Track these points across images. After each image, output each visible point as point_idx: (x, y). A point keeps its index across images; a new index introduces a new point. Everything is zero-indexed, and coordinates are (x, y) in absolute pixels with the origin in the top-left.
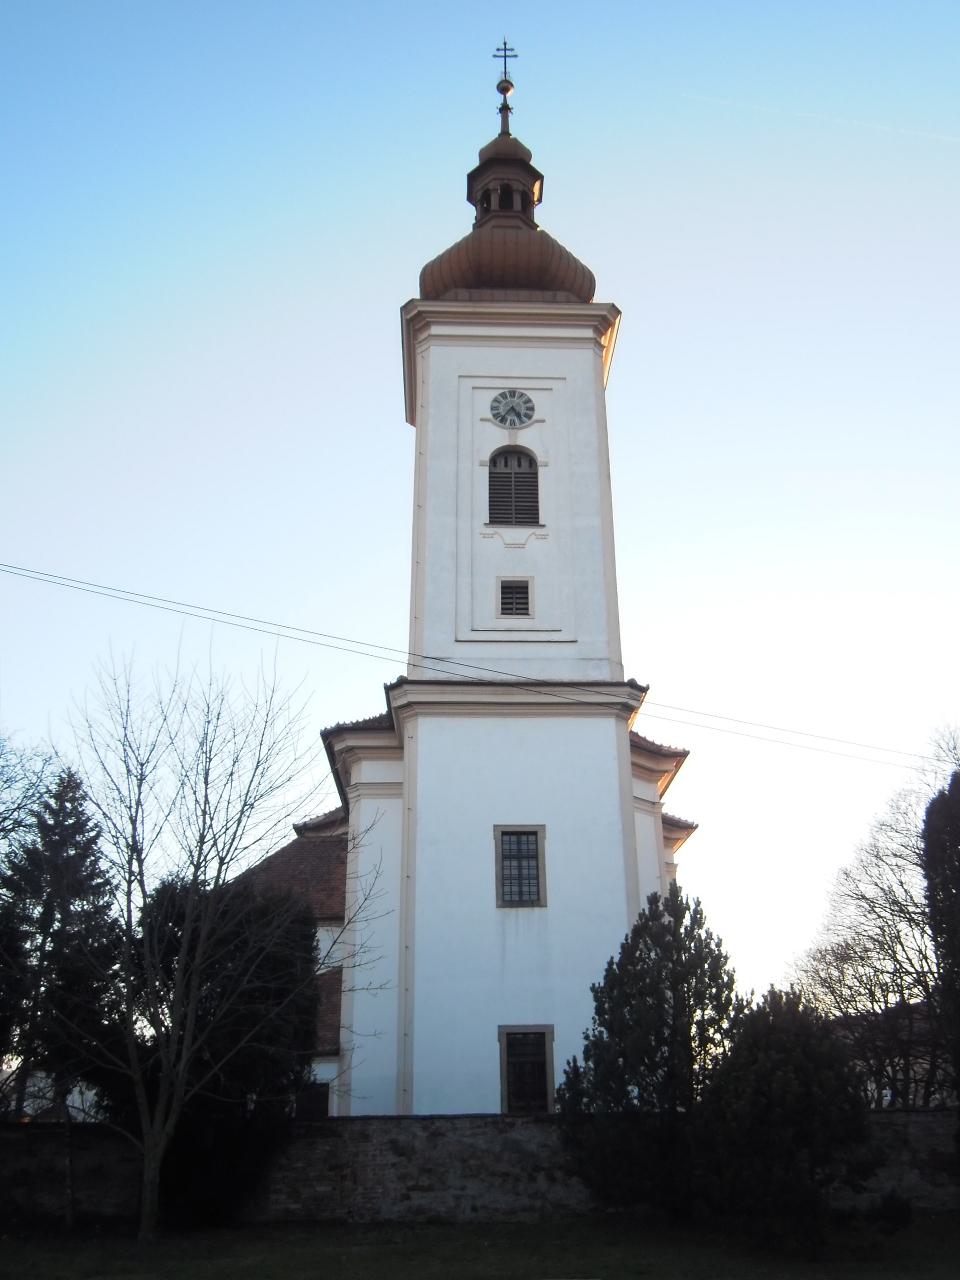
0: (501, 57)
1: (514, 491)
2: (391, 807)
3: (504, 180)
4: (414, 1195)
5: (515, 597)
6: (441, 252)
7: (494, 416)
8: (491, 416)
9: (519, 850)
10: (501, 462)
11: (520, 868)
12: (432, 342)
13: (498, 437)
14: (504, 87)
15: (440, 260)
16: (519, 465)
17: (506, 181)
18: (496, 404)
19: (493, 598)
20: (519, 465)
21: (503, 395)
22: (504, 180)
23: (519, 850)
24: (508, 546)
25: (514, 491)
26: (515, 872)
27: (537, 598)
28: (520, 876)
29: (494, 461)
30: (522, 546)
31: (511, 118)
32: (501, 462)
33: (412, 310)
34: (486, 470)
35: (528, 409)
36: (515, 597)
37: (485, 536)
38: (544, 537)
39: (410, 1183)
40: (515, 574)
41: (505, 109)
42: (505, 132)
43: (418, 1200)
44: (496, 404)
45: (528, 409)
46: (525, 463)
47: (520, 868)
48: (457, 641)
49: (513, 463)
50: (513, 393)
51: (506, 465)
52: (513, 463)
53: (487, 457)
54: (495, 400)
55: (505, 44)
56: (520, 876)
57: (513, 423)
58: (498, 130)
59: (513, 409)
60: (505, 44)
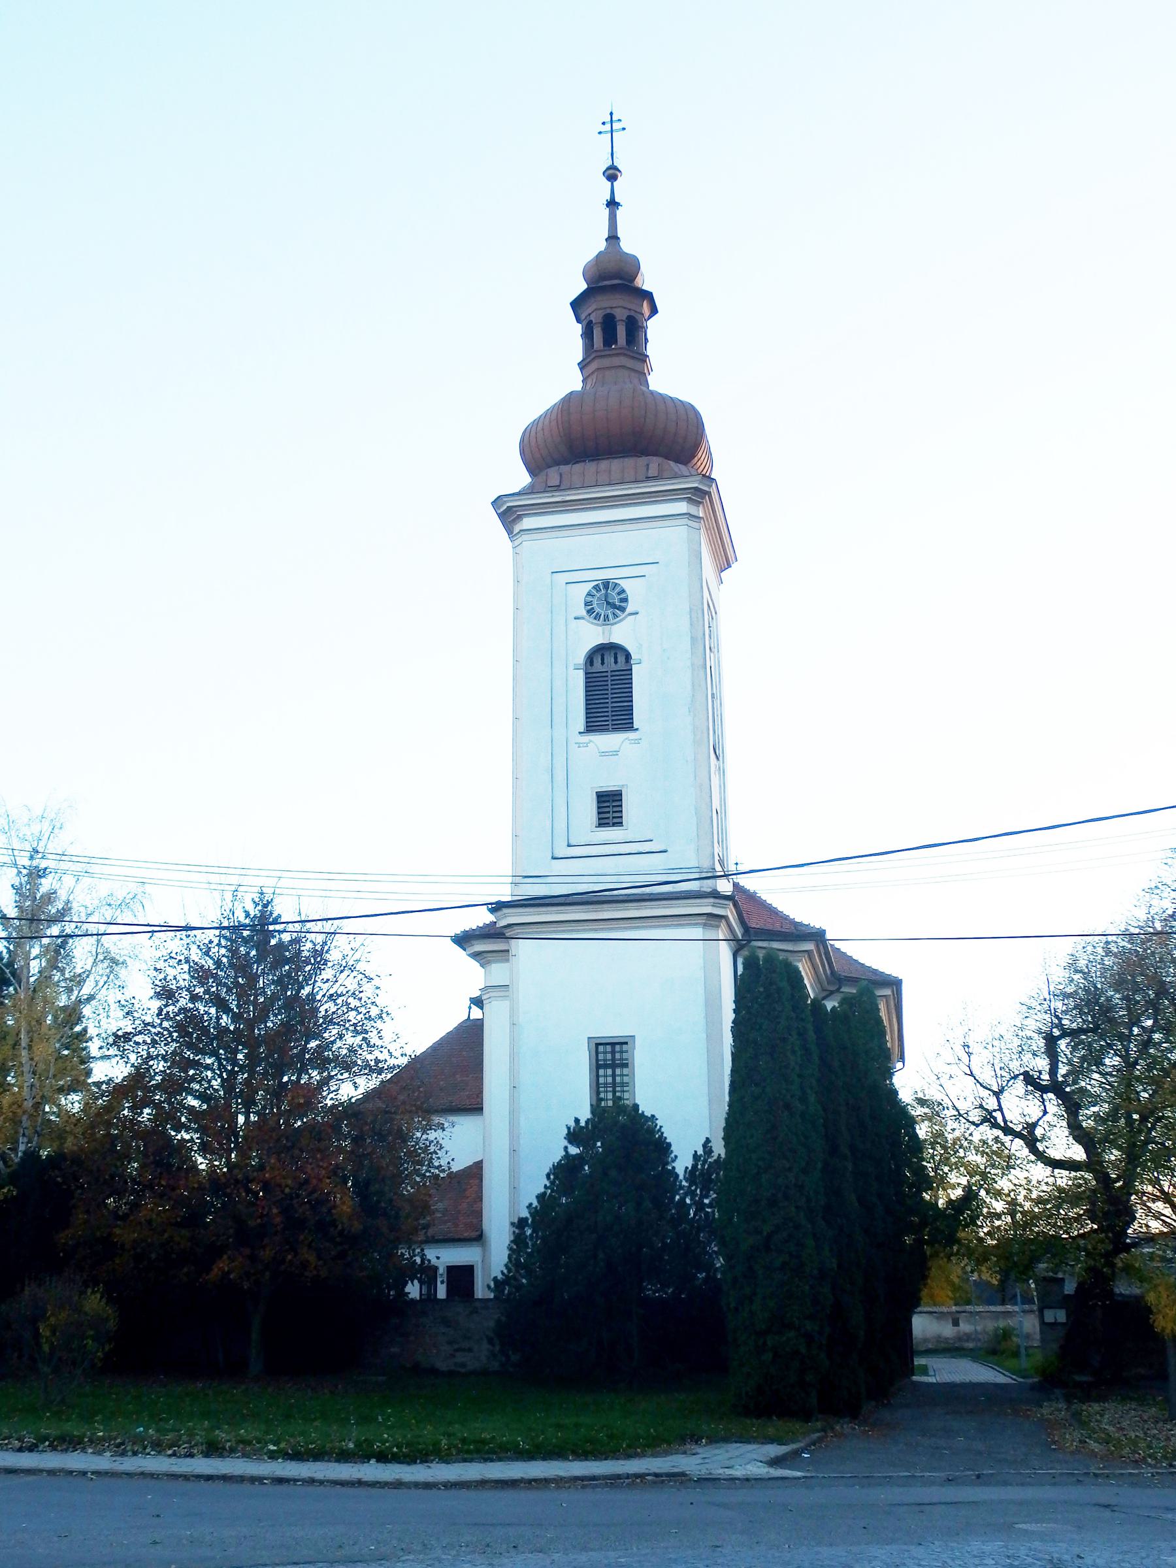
0: (606, 132)
1: (608, 695)
2: (505, 1004)
3: (614, 307)
4: (458, 1354)
5: (609, 807)
6: (536, 416)
7: (588, 612)
8: (584, 613)
9: (613, 1059)
10: (597, 660)
11: (614, 1076)
12: (525, 537)
13: (593, 635)
14: (612, 174)
15: (536, 423)
16: (616, 662)
17: (608, 311)
18: (590, 599)
19: (588, 809)
20: (616, 662)
21: (596, 588)
22: (614, 307)
23: (613, 1059)
24: (604, 754)
25: (608, 695)
26: (610, 1080)
27: (630, 808)
28: (614, 1083)
29: (590, 659)
30: (615, 753)
31: (620, 213)
32: (597, 660)
33: (502, 505)
34: (580, 677)
35: (619, 594)
36: (609, 807)
37: (579, 745)
38: (638, 741)
39: (456, 1346)
40: (609, 785)
41: (612, 204)
42: (613, 238)
43: (460, 1358)
44: (590, 599)
45: (619, 594)
46: (621, 659)
47: (614, 1076)
48: (554, 858)
49: (610, 659)
50: (606, 584)
51: (603, 663)
52: (610, 659)
53: (581, 658)
54: (589, 594)
55: (611, 114)
56: (614, 1083)
57: (606, 618)
58: (602, 245)
59: (608, 600)
60: (611, 114)
